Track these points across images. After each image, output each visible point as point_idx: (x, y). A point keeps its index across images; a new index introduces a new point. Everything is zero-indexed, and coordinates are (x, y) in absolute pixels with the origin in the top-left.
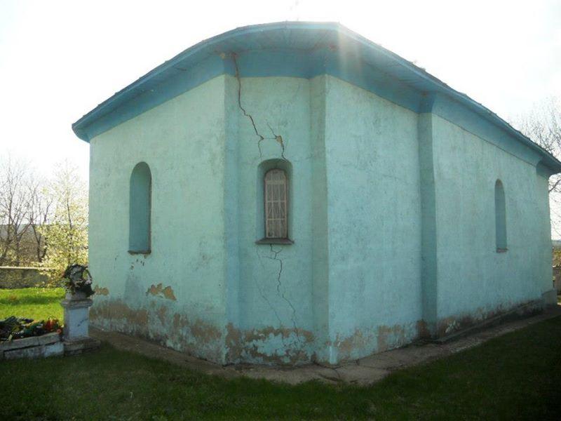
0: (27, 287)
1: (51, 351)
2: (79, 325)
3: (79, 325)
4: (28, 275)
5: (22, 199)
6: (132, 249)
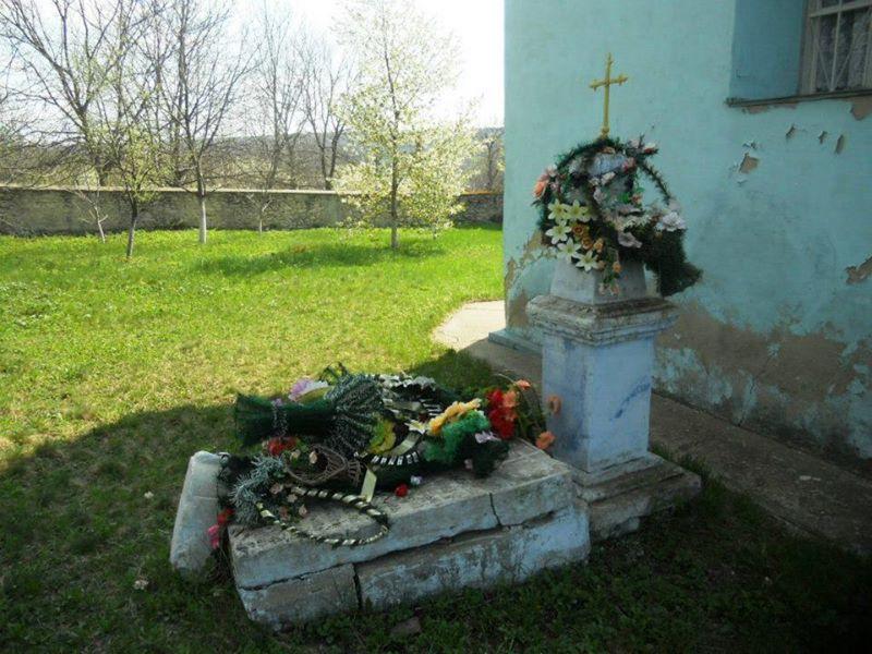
0: (317, 226)
1: (548, 547)
2: (620, 414)
3: (620, 414)
4: (317, 205)
5: (290, 69)
6: (741, 93)
